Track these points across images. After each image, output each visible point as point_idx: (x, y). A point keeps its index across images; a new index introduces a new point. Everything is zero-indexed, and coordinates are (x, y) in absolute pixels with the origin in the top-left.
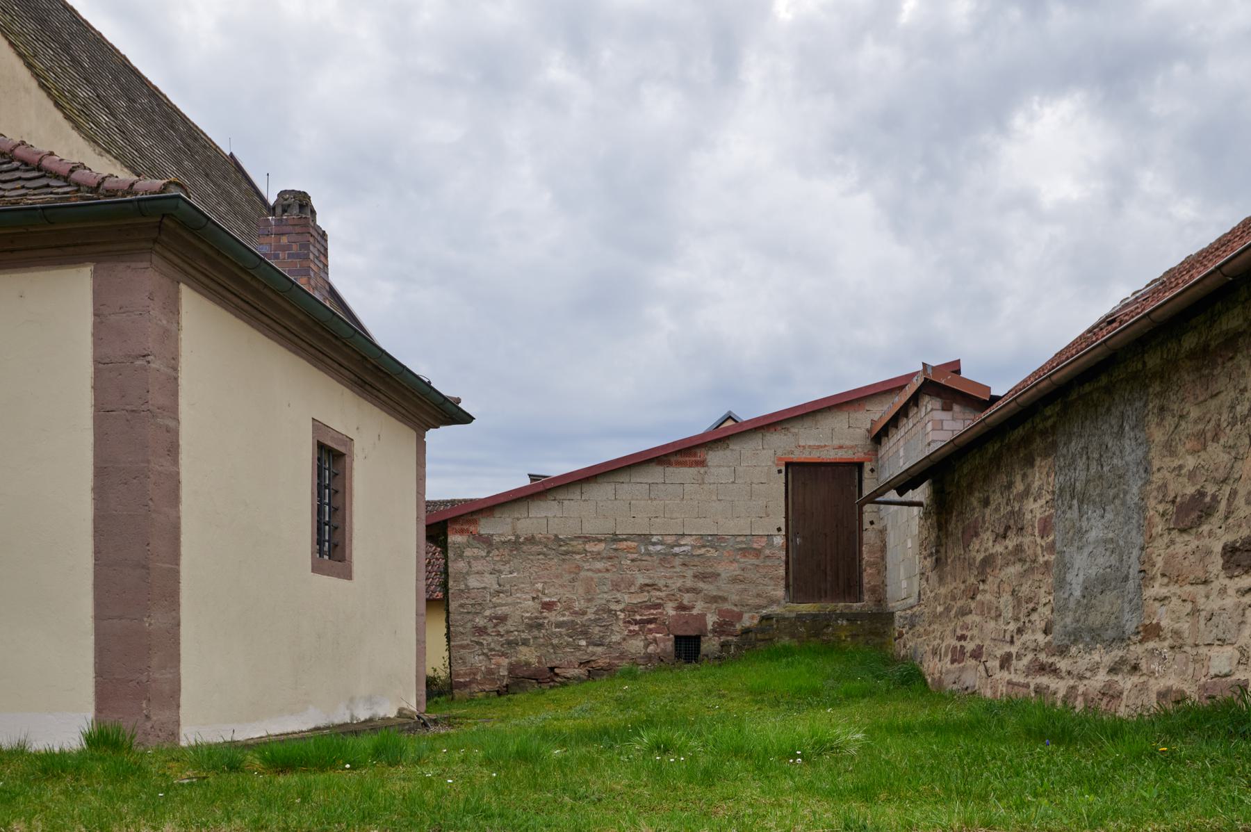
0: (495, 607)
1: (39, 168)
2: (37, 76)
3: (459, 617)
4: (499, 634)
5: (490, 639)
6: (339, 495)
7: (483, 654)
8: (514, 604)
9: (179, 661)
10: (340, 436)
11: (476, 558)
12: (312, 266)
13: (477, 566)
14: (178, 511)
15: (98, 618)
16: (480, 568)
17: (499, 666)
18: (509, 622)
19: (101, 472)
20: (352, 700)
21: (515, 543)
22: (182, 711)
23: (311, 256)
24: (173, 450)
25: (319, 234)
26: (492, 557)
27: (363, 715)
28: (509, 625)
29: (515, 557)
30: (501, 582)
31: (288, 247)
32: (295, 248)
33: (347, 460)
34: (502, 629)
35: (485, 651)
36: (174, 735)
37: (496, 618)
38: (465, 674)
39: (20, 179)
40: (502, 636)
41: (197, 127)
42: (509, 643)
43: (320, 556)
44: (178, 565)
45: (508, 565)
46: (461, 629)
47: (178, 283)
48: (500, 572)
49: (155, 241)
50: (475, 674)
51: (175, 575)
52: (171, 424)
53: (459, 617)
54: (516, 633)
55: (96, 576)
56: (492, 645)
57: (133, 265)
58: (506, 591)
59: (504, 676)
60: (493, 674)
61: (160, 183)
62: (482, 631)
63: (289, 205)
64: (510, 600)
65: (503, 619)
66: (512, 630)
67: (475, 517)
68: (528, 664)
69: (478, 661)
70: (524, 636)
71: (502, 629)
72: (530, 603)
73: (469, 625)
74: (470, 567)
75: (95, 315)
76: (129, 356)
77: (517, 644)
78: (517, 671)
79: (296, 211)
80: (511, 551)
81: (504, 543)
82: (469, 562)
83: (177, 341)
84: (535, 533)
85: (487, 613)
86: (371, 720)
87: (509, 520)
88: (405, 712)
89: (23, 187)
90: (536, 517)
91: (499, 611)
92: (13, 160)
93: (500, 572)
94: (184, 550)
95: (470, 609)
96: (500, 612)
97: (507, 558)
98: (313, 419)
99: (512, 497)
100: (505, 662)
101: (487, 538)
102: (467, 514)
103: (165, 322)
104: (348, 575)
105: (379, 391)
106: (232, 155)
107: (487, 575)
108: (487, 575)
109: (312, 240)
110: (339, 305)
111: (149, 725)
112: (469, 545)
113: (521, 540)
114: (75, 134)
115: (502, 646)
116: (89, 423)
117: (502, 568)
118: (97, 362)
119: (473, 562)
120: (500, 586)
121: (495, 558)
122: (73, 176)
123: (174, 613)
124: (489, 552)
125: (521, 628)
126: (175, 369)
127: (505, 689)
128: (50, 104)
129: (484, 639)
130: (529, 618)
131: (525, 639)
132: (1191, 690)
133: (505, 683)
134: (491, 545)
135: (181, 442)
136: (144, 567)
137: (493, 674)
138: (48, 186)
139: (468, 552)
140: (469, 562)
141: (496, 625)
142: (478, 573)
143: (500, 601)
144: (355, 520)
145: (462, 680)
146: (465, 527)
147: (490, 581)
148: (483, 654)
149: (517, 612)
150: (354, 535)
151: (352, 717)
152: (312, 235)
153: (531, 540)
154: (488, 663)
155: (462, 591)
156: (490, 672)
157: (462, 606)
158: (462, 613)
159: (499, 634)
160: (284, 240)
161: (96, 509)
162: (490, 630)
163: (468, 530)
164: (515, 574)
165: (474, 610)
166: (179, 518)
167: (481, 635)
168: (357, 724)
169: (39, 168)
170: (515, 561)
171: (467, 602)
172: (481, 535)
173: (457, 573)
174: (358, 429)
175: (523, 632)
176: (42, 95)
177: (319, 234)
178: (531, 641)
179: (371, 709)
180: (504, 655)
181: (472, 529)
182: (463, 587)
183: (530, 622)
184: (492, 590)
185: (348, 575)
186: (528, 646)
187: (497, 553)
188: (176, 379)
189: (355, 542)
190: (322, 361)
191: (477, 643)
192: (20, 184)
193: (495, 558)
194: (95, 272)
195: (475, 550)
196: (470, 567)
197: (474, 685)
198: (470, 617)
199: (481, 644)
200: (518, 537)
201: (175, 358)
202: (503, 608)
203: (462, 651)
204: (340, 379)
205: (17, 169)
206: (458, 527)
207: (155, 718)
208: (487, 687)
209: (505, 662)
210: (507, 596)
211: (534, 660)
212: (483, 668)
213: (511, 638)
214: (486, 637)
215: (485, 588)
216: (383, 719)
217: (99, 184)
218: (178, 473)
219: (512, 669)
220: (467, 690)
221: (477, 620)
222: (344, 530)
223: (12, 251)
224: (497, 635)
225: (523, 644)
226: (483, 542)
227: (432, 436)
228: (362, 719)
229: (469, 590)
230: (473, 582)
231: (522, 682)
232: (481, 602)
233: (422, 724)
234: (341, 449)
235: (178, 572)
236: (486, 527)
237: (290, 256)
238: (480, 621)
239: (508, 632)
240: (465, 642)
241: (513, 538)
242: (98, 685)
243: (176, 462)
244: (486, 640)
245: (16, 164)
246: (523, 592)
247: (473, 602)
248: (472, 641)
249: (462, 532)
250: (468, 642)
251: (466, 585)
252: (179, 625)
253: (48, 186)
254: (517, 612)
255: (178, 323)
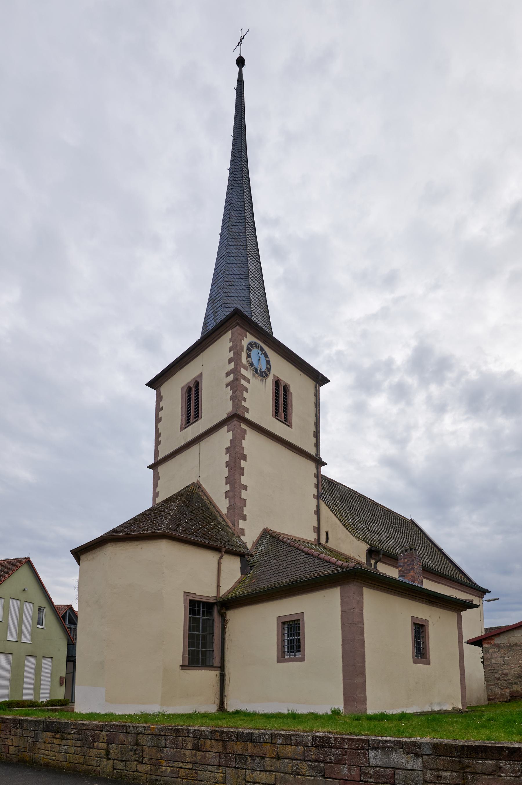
0: (503, 670)
1: (329, 562)
2: (341, 522)
3: (489, 674)
4: (505, 680)
5: (501, 682)
6: (424, 638)
7: (499, 688)
8: (511, 669)
9: (366, 691)
10: (423, 620)
11: (494, 652)
12: (415, 567)
13: (495, 655)
14: (364, 649)
15: (344, 679)
16: (496, 656)
17: (506, 692)
18: (509, 676)
19: (343, 640)
20: (431, 704)
21: (509, 646)
22: (367, 706)
23: (415, 564)
24: (362, 633)
25: (417, 556)
26: (501, 652)
27: (436, 708)
28: (509, 677)
29: (510, 651)
30: (505, 661)
31: (407, 562)
32: (409, 562)
33: (426, 626)
34: (506, 678)
35: (500, 687)
36: (365, 712)
37: (504, 674)
38: (492, 695)
39: (325, 565)
40: (506, 681)
41: (398, 514)
42: (509, 683)
43: (417, 658)
44: (365, 664)
45: (507, 655)
46: (490, 678)
47: (362, 587)
48: (504, 657)
49: (354, 578)
50: (496, 695)
51: (364, 668)
52: (361, 626)
53: (489, 674)
54: (512, 680)
55: (343, 668)
56: (502, 684)
57: (349, 585)
58: (507, 664)
59: (508, 696)
60: (504, 695)
61: (354, 564)
62: (498, 679)
63: (407, 550)
64: (509, 667)
65: (506, 675)
66: (510, 678)
67: (493, 637)
68: (517, 691)
69: (497, 690)
70: (515, 681)
71: (506, 678)
72: (517, 668)
73: (493, 677)
74: (492, 656)
75: (341, 599)
76: (349, 609)
77: (513, 684)
78: (513, 694)
79: (409, 551)
80: (508, 649)
81: (505, 646)
82: (491, 654)
83: (362, 602)
84: (517, 642)
85: (500, 672)
86: (440, 710)
87: (506, 638)
88: (455, 708)
89: (325, 568)
90: (517, 636)
91: (505, 672)
92: (324, 560)
93: (504, 657)
94: (366, 660)
95: (493, 671)
96: (505, 672)
97: (507, 652)
98: (411, 616)
99: (514, 627)
100: (508, 690)
101: (498, 645)
102: (490, 636)
103: (358, 599)
104: (429, 663)
105: (438, 603)
106: (411, 519)
107: (499, 658)
108: (499, 658)
109: (414, 559)
110: (451, 563)
111: (357, 709)
112: (491, 648)
113: (512, 645)
114: (351, 536)
115: (506, 684)
116: (340, 628)
117: (505, 656)
118: (342, 611)
119: (493, 654)
120: (504, 662)
121: (502, 652)
122: (336, 563)
123: (364, 678)
124: (499, 650)
125: (514, 678)
126: (362, 611)
127: (509, 701)
128: (345, 529)
129: (499, 682)
130: (517, 674)
131: (515, 682)
132: (336, 708)
133: (508, 699)
134: (500, 647)
135: (365, 630)
136: (354, 665)
137: (504, 695)
138: (331, 567)
139: (491, 651)
140: (491, 654)
141: (503, 677)
142: (495, 658)
143: (505, 668)
144: (430, 645)
145: (491, 697)
146: (489, 641)
147: (500, 660)
148: (499, 688)
149: (512, 672)
150: (430, 650)
151: (432, 709)
152: (414, 557)
153: (516, 645)
154: (501, 691)
155: (489, 665)
156: (502, 694)
157: (490, 670)
158: (490, 673)
159: (505, 680)
160: (406, 560)
161: (343, 650)
162: (501, 679)
163: (490, 643)
164: (510, 658)
165: (494, 672)
166: (365, 651)
167: (497, 681)
168: (434, 712)
169: (329, 562)
170: (510, 653)
171: (491, 668)
172: (495, 644)
173: (486, 658)
174: (430, 616)
175: (515, 679)
176: (343, 527)
177: (417, 556)
178: (518, 683)
179: (440, 707)
180: (507, 688)
181: (492, 642)
182: (489, 663)
183: (518, 675)
184: (501, 664)
185: (429, 663)
186: (517, 685)
187: (502, 650)
188: (363, 613)
189: (431, 653)
190: (414, 598)
191: (496, 684)
192: (325, 567)
193: (502, 652)
194: (340, 589)
195: (494, 650)
196: (492, 656)
197: (496, 699)
198: (492, 674)
199: (498, 684)
200: (510, 644)
201: (362, 608)
202: (506, 670)
203: (491, 687)
204: (422, 602)
205: (324, 563)
206: (486, 641)
207: (358, 707)
208: (501, 700)
209: (508, 690)
210: (508, 666)
211: (519, 690)
212: (499, 693)
213: (510, 682)
214: (500, 682)
215: (498, 663)
216: (445, 710)
217: (342, 565)
218: (364, 639)
219: (511, 693)
220: (494, 701)
221: (496, 675)
222: (426, 649)
223: (322, 585)
224: (504, 681)
225: (515, 684)
226: (497, 647)
227: (464, 613)
228: (436, 710)
229: (492, 664)
230: (493, 661)
231: (516, 698)
232: (497, 668)
233: (461, 712)
234: (424, 624)
235: (365, 666)
236: (497, 641)
237: (408, 565)
238: (497, 676)
239: (509, 679)
240: (492, 683)
241: (509, 644)
242: (344, 698)
243: (363, 636)
244: (500, 683)
245: (324, 561)
246: (514, 664)
247: (494, 668)
248: (494, 683)
249: (488, 643)
250: (493, 683)
251: (491, 662)
252: (365, 681)
253: (331, 567)
254: (512, 672)
255: (363, 598)
